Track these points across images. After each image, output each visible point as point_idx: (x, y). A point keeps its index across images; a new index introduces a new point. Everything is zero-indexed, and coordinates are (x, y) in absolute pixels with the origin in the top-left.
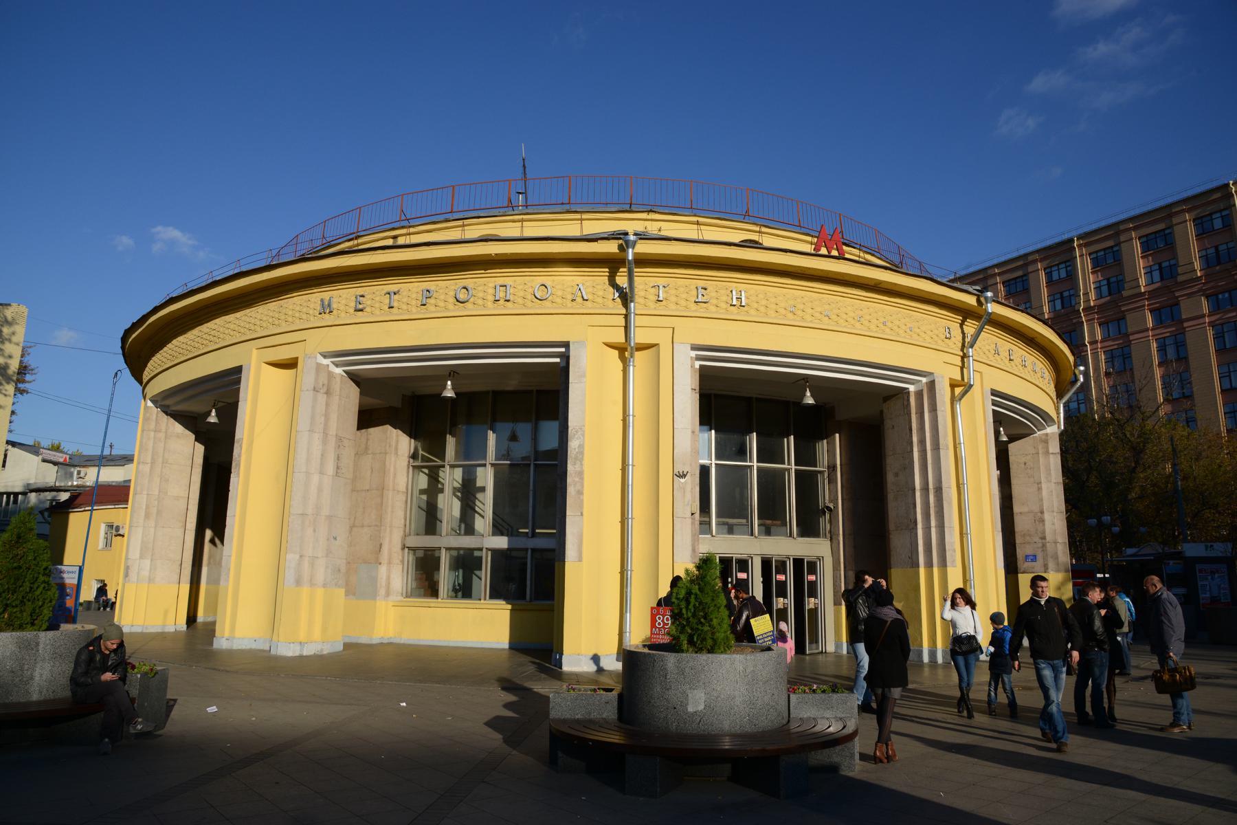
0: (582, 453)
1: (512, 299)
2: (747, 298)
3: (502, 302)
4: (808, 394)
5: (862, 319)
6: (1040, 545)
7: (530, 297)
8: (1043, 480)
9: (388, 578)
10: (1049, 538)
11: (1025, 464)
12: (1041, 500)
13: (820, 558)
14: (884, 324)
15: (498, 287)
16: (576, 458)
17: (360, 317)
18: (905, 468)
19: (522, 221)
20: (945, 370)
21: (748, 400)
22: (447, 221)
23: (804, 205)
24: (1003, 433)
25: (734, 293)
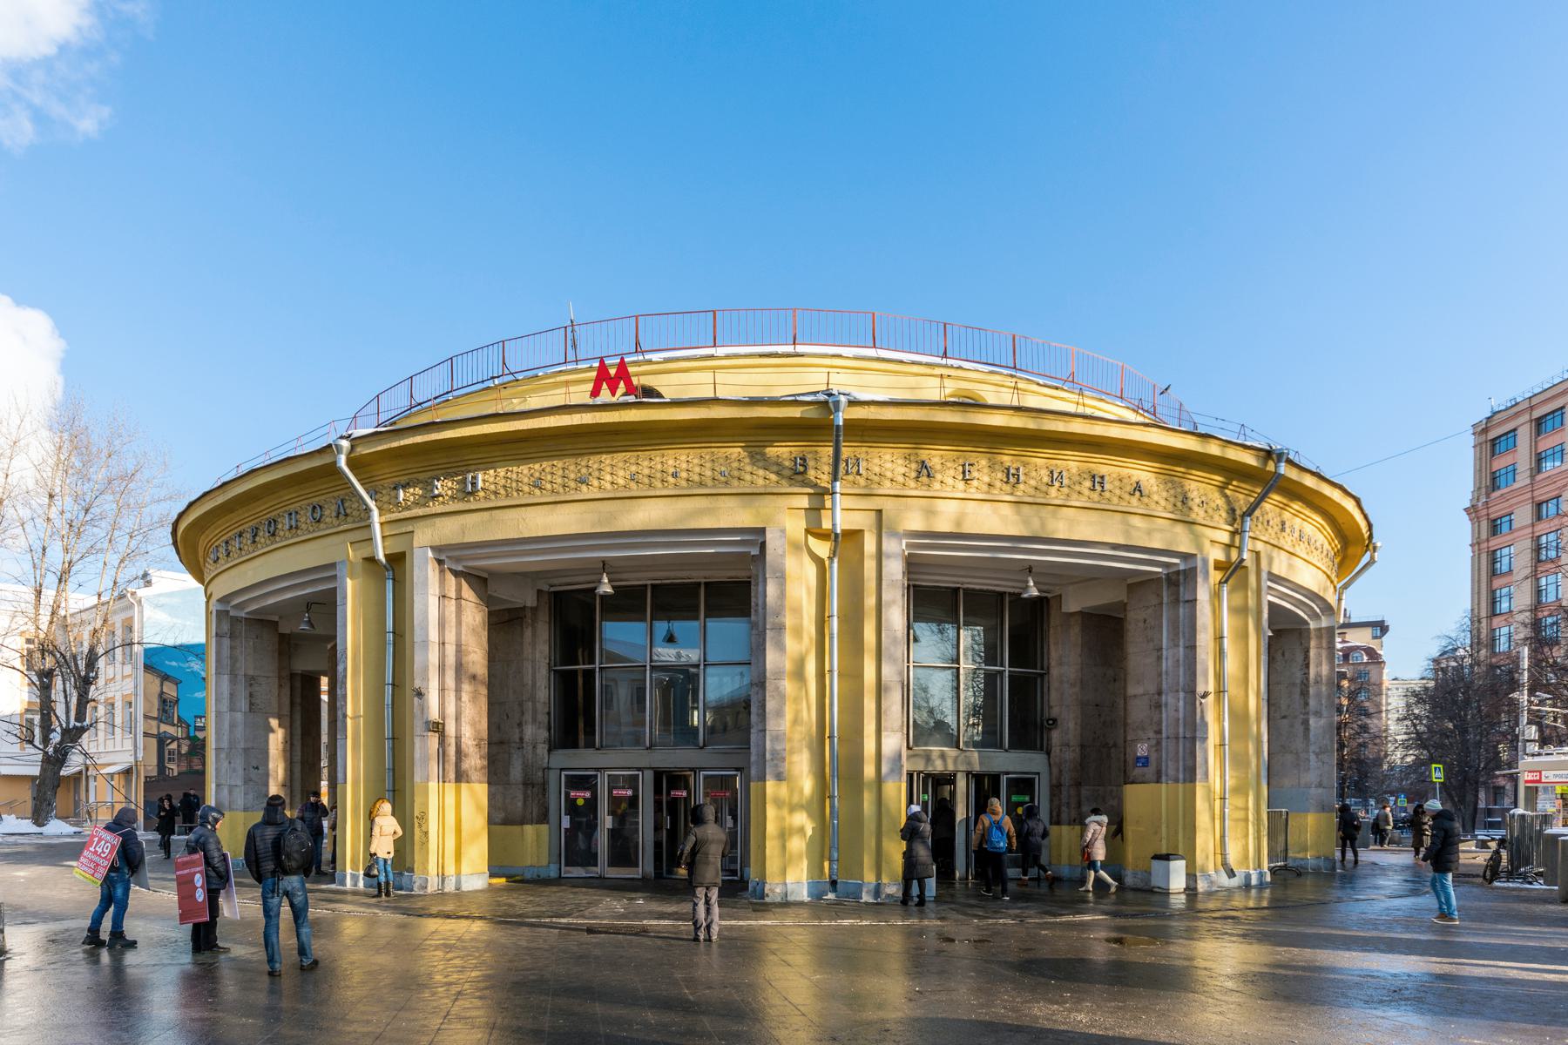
6: (1154, 742)
11: (1145, 621)
19: (567, 383)
23: (996, 335)
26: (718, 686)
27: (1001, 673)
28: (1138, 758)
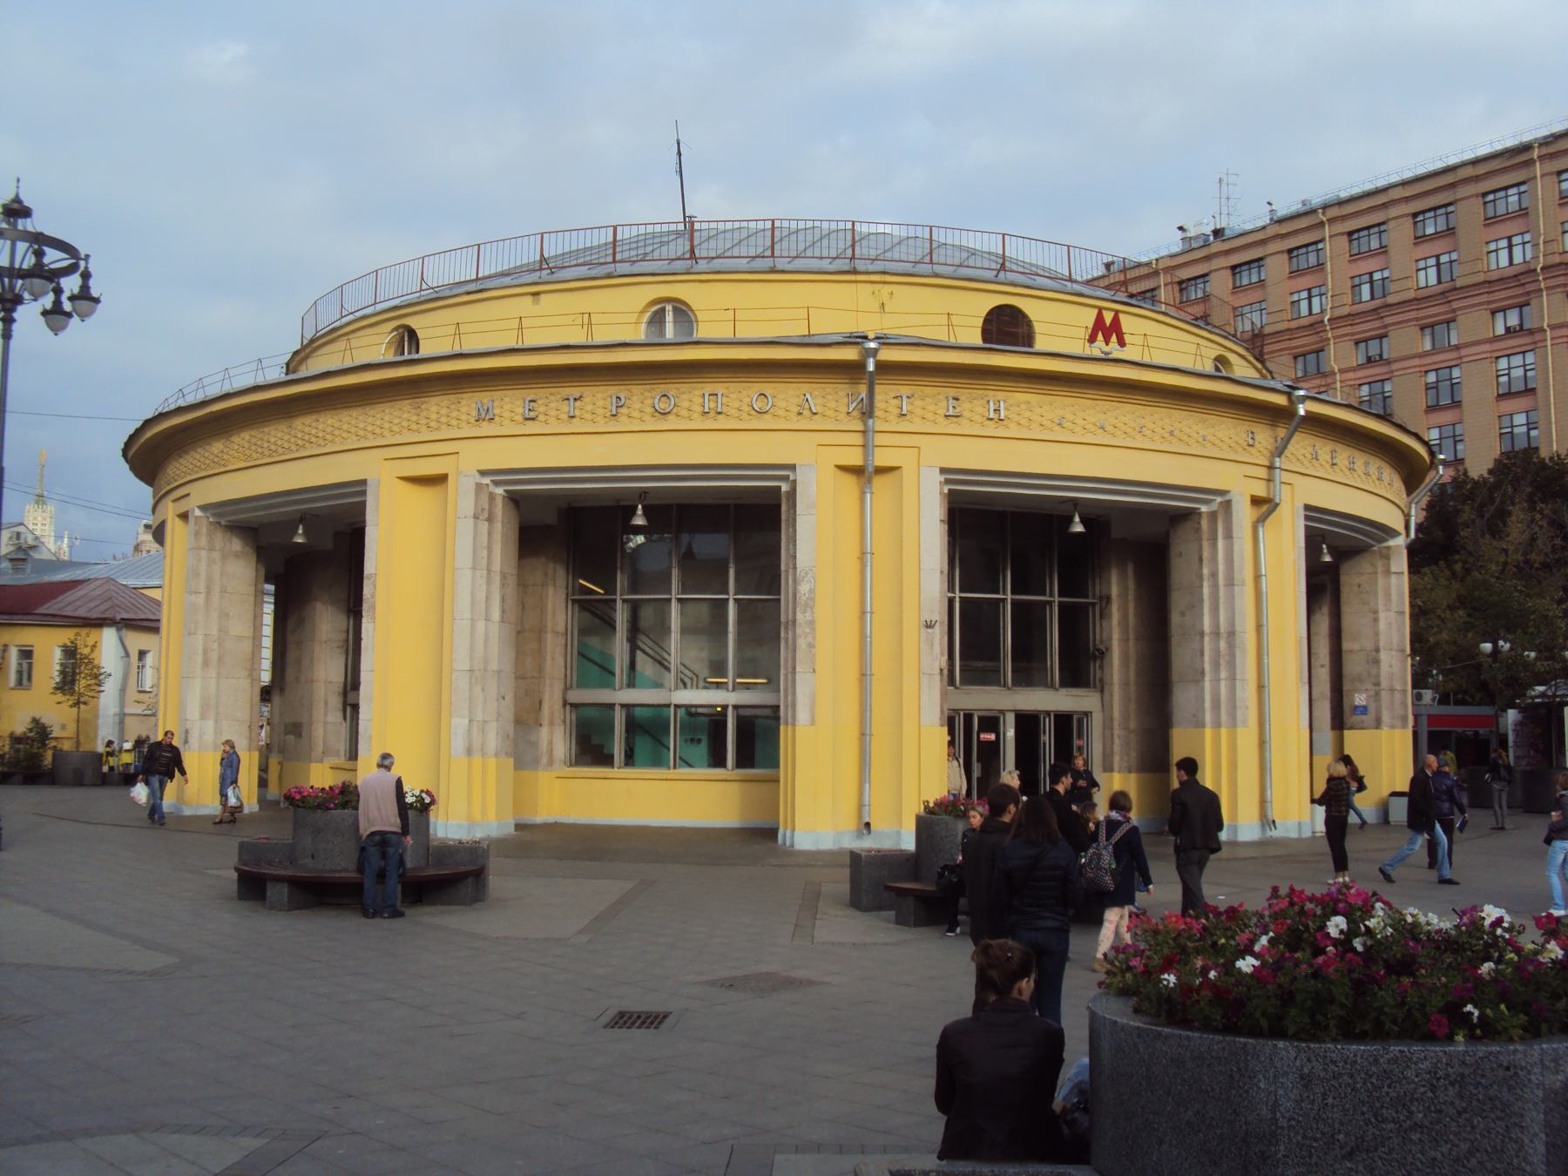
0: (812, 599)
1: (724, 410)
2: (1006, 409)
3: (712, 414)
4: (1077, 519)
5: (1144, 429)
6: (1372, 693)
7: (746, 408)
8: (1381, 607)
9: (551, 742)
10: (1384, 683)
11: (1359, 586)
12: (1377, 634)
13: (1087, 714)
14: (1171, 433)
15: (707, 397)
16: (806, 605)
17: (531, 428)
18: (1193, 607)
20: (1241, 484)
21: (1002, 515)
22: (609, 276)
24: (1325, 551)
25: (991, 403)
26: (1428, 695)
27: (1004, 600)
28: (1356, 707)
